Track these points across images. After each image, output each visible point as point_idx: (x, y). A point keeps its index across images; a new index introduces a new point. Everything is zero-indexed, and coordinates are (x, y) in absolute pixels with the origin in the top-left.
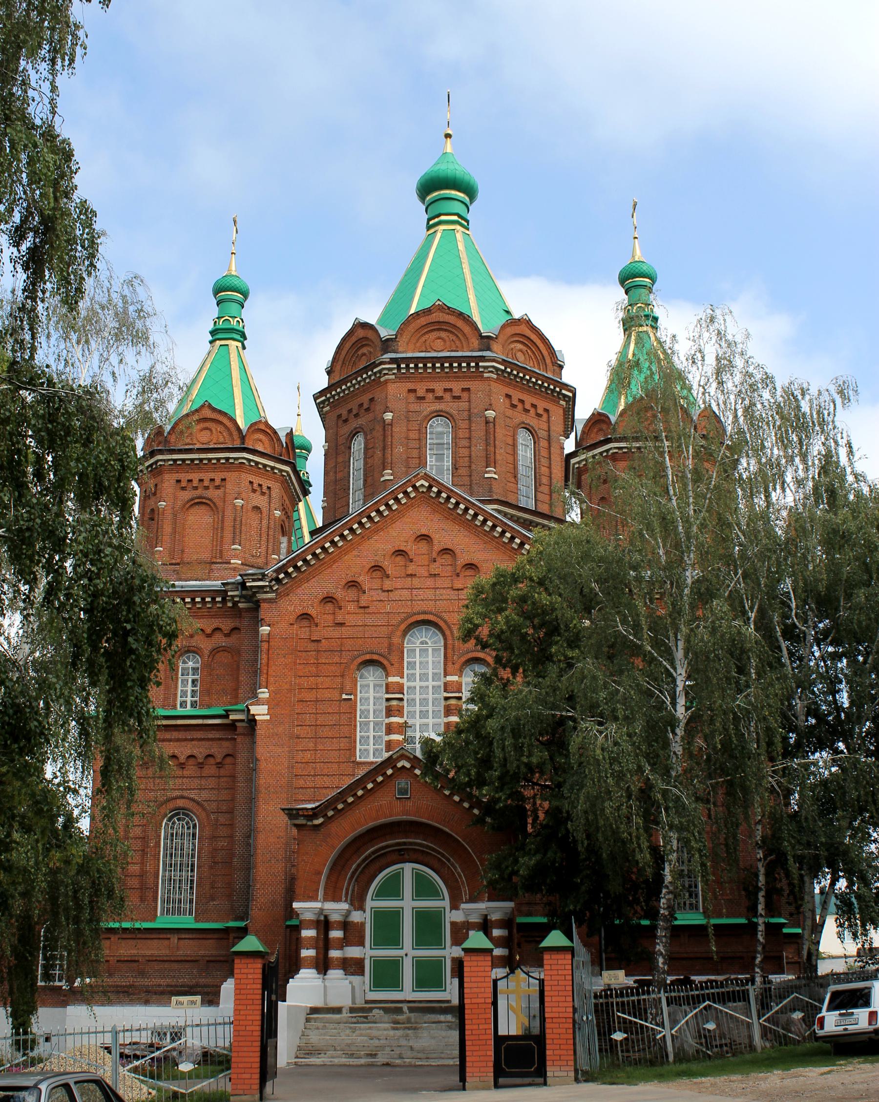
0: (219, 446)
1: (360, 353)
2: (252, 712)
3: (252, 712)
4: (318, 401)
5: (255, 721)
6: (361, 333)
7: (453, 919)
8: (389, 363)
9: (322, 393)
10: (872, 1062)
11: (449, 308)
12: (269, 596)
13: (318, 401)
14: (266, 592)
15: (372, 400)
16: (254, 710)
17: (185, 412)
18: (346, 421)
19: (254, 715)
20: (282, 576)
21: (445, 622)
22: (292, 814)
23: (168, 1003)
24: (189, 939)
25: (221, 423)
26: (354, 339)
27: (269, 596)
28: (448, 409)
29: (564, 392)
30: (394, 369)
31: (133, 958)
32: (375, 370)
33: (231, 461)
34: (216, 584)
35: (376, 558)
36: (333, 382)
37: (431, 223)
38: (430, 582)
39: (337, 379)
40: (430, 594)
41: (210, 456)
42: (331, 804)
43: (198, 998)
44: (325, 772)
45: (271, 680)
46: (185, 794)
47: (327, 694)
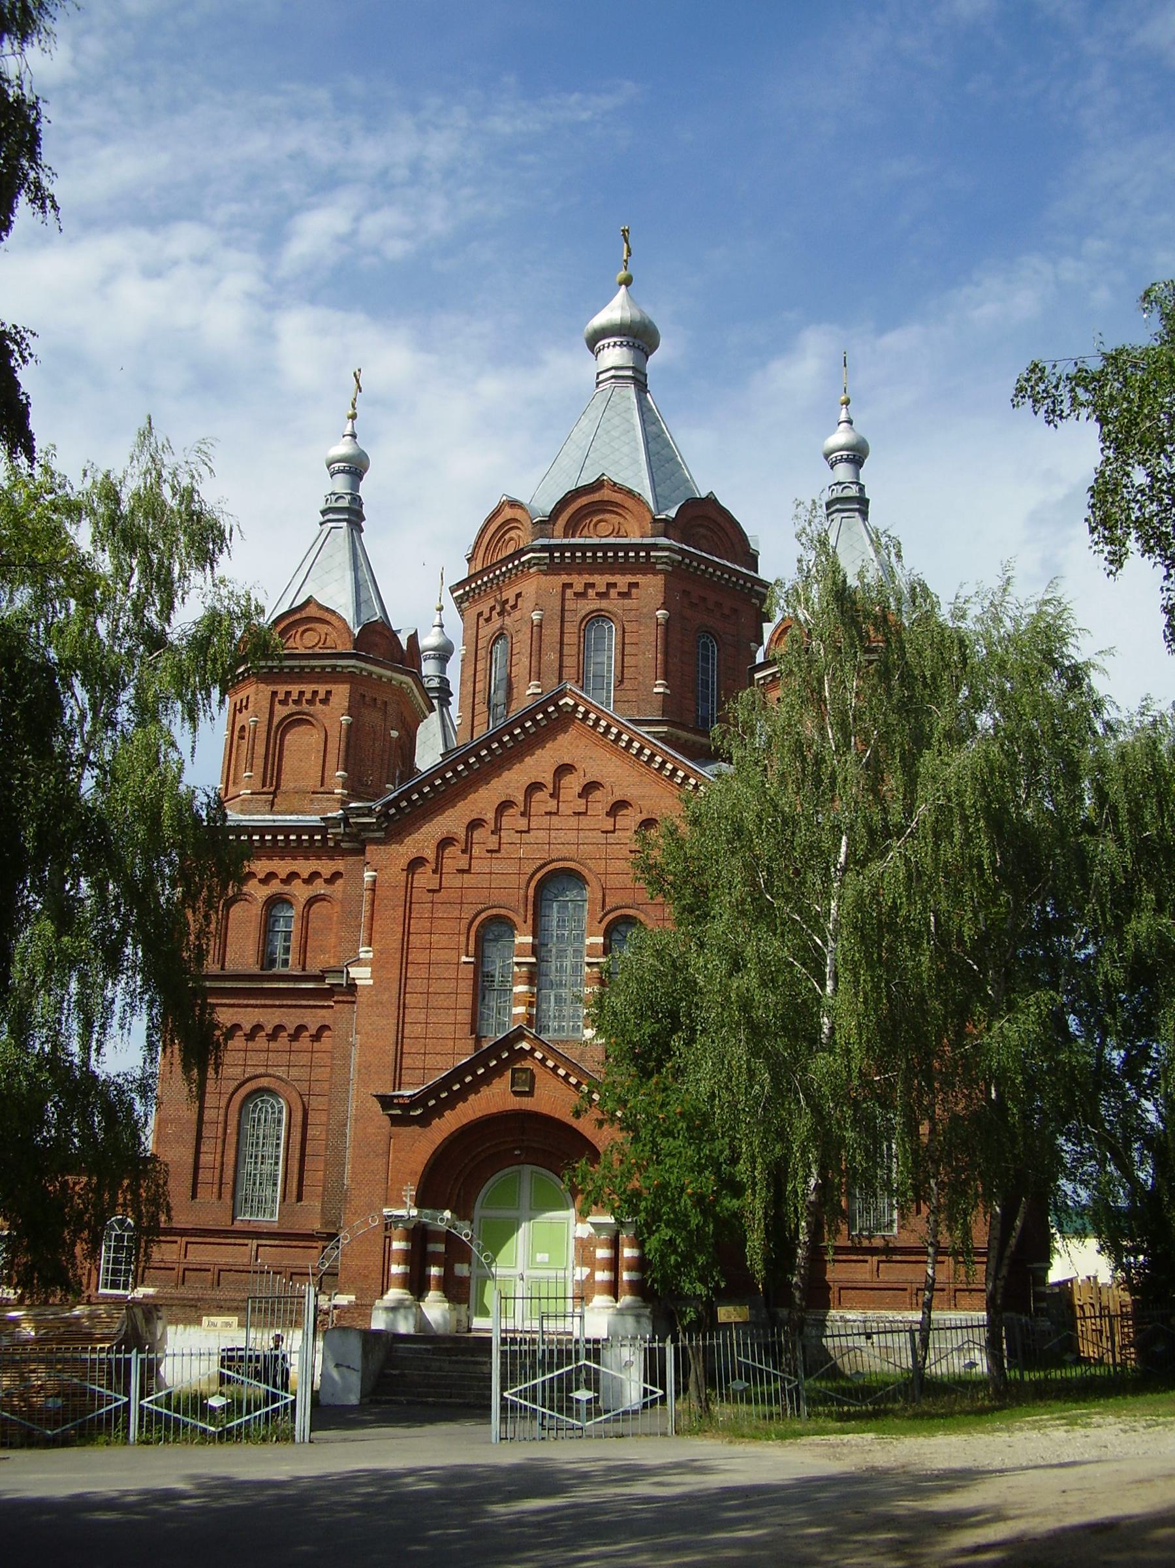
0: (326, 651)
1: (507, 537)
2: (351, 976)
3: (351, 976)
4: (456, 594)
5: (356, 985)
6: (508, 513)
7: (578, 1234)
8: (540, 551)
9: (460, 585)
10: (1072, 1422)
11: (615, 484)
12: (377, 835)
13: (456, 594)
14: (373, 831)
15: (519, 595)
16: (354, 972)
17: (286, 609)
18: (488, 620)
19: (354, 979)
20: (392, 811)
21: (590, 870)
22: (386, 1102)
23: (199, 1322)
24: (271, 1246)
25: (328, 623)
26: (499, 520)
27: (377, 835)
28: (610, 608)
29: (756, 587)
30: (545, 558)
31: (203, 1267)
32: (523, 559)
33: (339, 669)
34: (313, 819)
35: (509, 791)
36: (473, 572)
37: (602, 377)
38: (573, 822)
39: (479, 568)
40: (572, 836)
41: (304, 663)
42: (432, 1091)
43: (234, 1320)
44: (438, 1049)
45: (376, 936)
46: (270, 1071)
47: (443, 956)
